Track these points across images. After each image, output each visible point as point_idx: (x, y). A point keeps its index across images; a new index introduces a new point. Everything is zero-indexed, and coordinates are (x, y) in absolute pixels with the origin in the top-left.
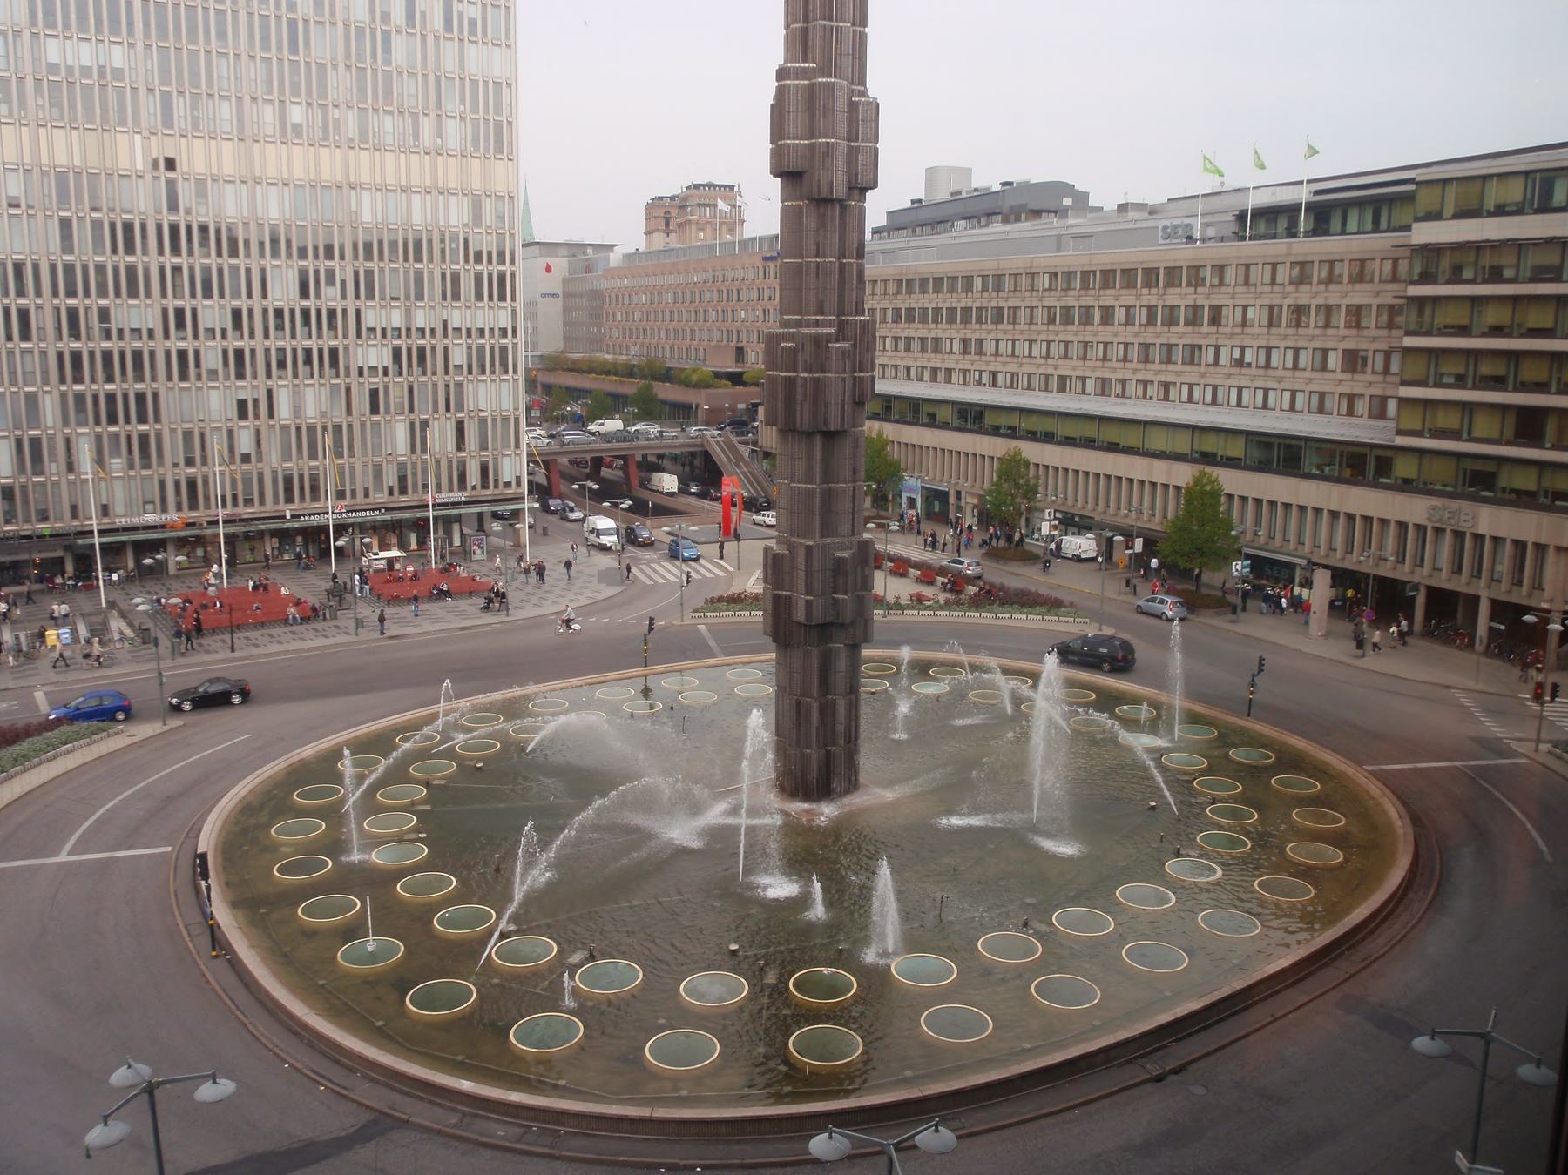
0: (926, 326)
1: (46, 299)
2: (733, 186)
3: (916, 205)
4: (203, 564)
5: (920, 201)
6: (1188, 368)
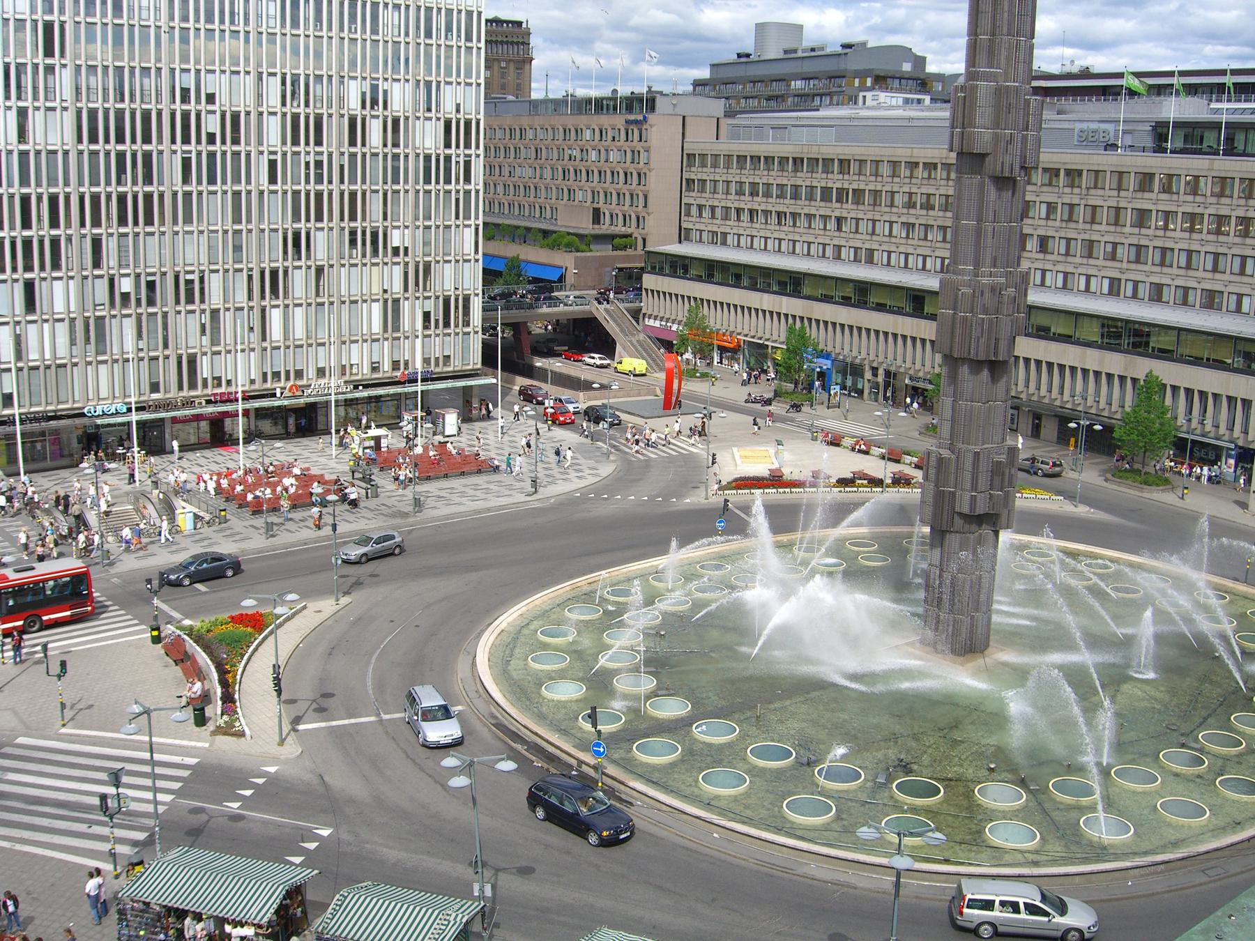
0: (829, 204)
1: (461, 151)
2: (522, 23)
3: (743, 60)
4: (1064, 850)
5: (748, 56)
6: (1109, 264)
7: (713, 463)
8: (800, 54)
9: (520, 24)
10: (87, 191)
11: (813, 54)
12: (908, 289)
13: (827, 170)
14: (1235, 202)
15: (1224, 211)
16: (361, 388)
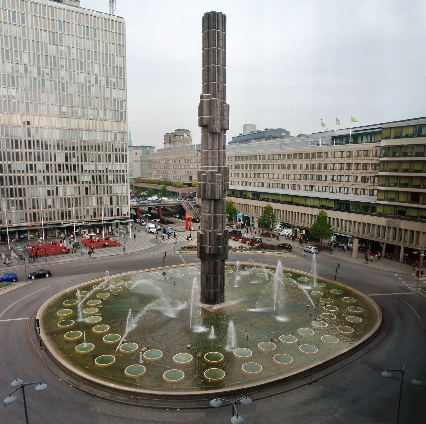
5: (242, 134)
7: (176, 242)
8: (254, 132)
9: (188, 130)
12: (251, 192)
15: (350, 162)
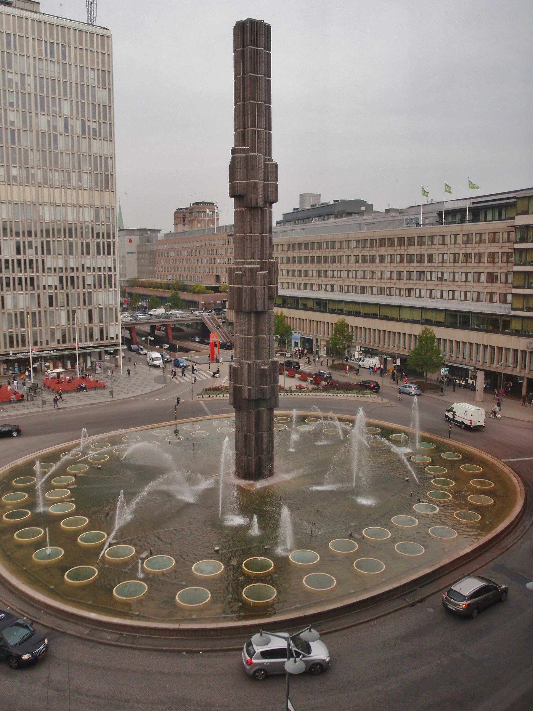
8: (317, 206)
10: (4, 276)
11: (323, 205)
13: (300, 249)
14: (474, 246)
15: (469, 251)
16: (55, 351)
